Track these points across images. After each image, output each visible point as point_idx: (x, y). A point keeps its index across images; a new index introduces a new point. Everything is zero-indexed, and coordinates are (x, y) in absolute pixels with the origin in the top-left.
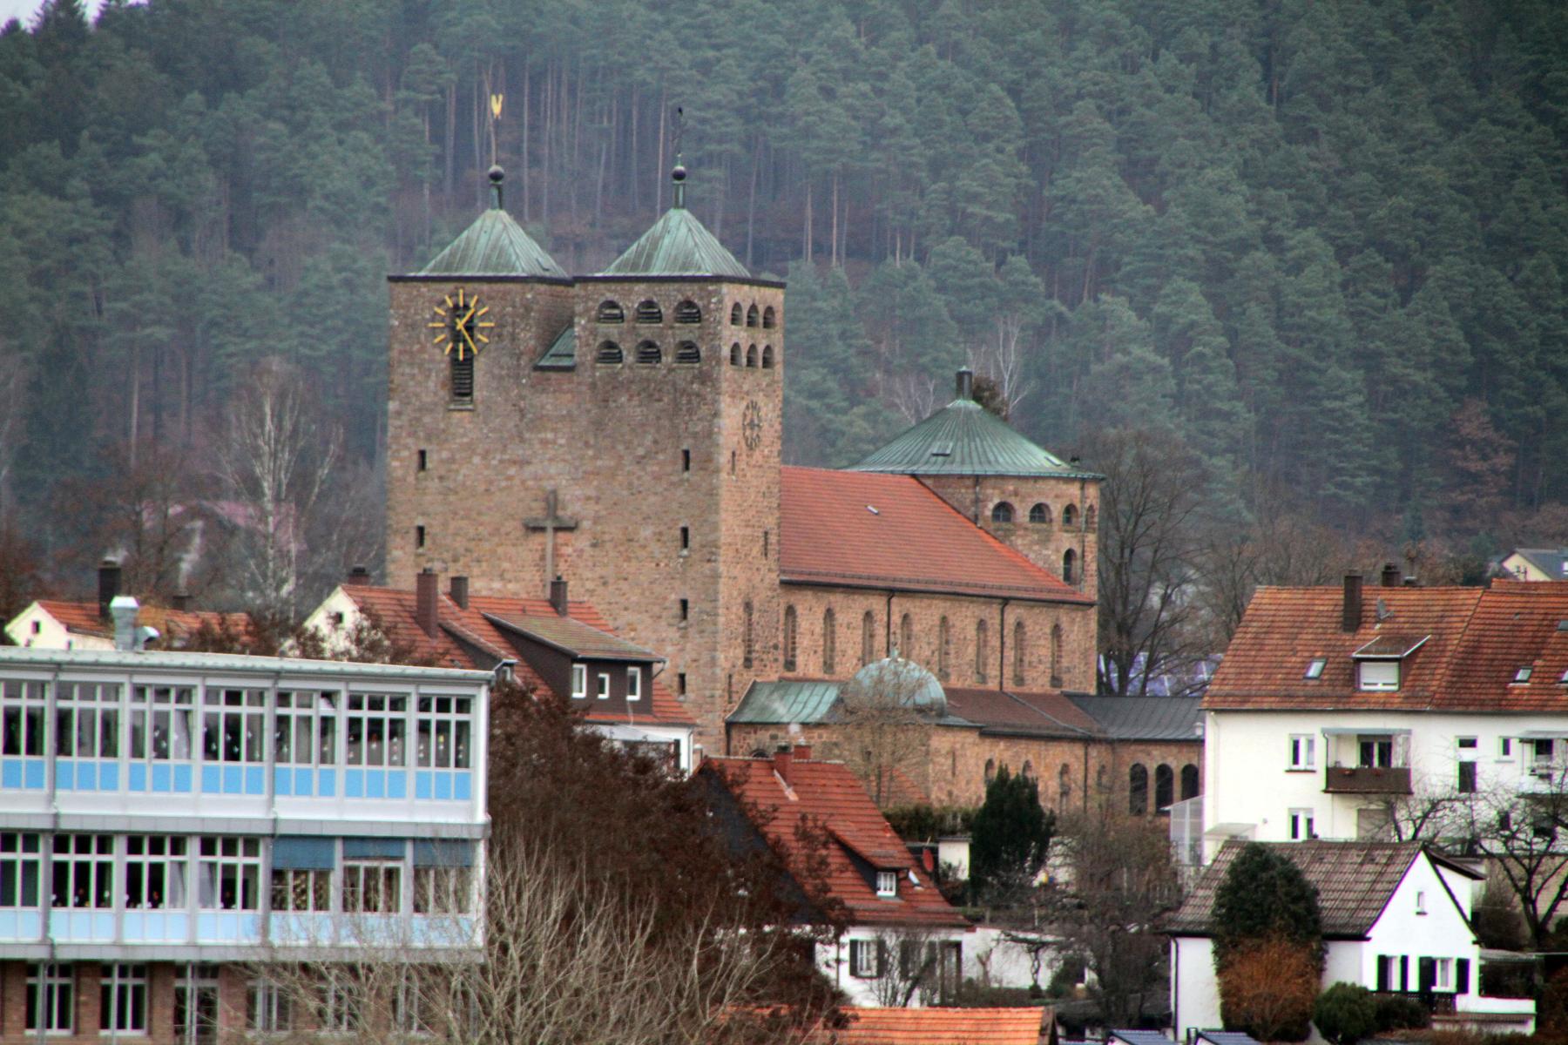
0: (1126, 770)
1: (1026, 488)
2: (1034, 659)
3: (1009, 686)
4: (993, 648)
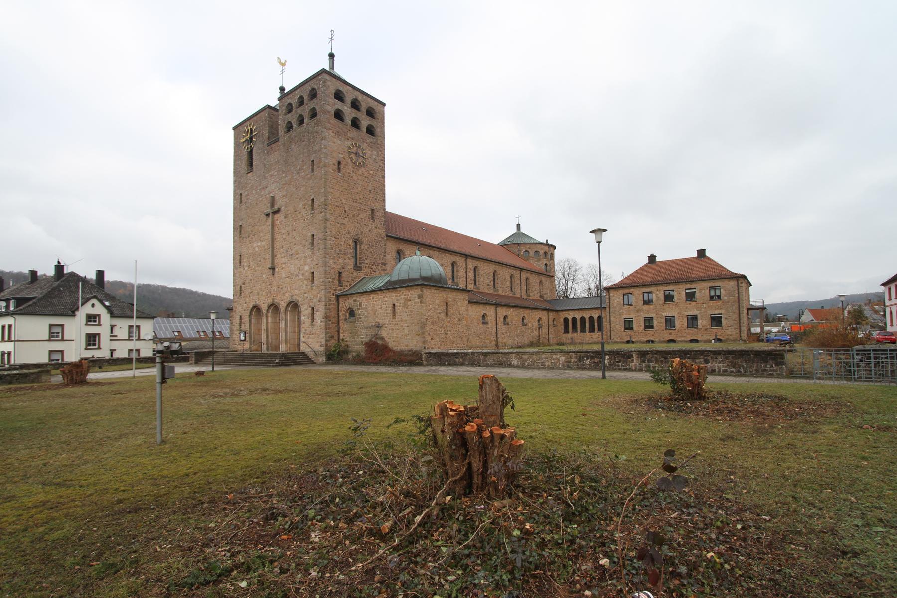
0: (562, 320)
2: (534, 289)
3: (524, 296)
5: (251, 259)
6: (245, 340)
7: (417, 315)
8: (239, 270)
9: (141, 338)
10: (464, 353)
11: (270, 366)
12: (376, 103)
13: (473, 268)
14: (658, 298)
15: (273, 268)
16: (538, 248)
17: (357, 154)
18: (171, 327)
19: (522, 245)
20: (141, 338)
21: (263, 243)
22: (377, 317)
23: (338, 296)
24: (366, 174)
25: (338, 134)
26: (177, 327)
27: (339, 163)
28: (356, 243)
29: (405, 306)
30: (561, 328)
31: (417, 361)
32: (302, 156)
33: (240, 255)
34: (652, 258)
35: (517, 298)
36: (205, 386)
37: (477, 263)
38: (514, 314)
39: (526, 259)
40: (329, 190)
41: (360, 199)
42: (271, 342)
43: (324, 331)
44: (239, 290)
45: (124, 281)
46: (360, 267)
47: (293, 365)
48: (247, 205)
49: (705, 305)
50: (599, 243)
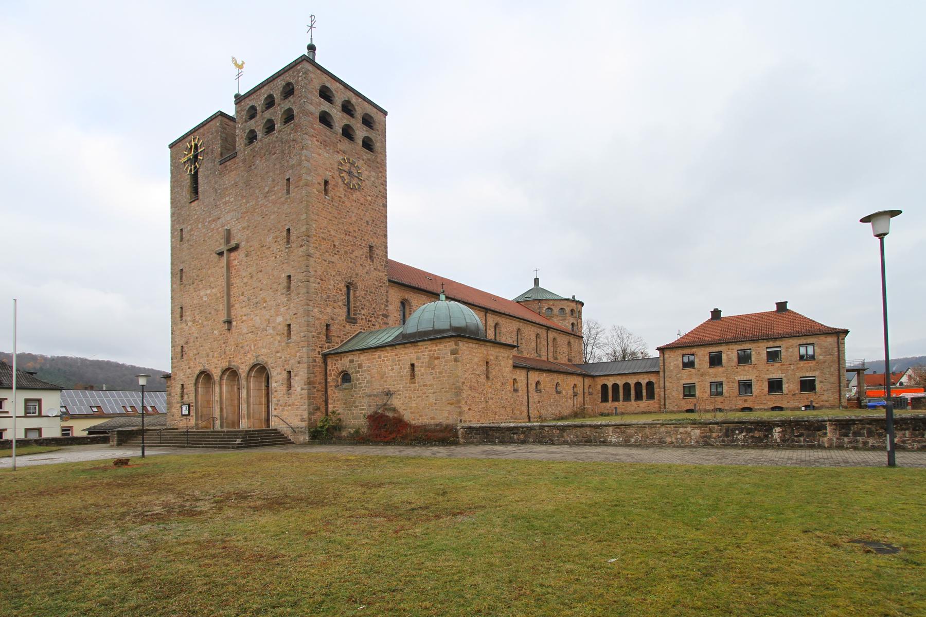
0: (599, 387)
1: (556, 303)
2: (561, 352)
3: (551, 359)
5: (197, 312)
6: (189, 414)
7: (449, 377)
8: (180, 327)
9: (43, 414)
11: (229, 448)
12: (375, 110)
13: (493, 325)
14: (729, 359)
15: (229, 322)
16: (564, 305)
17: (350, 173)
18: (88, 401)
20: (43, 414)
21: (213, 290)
22: (385, 381)
23: (325, 356)
24: (362, 200)
25: (324, 144)
26: (95, 401)
27: (326, 183)
28: (348, 288)
29: (431, 366)
31: (452, 439)
32: (271, 174)
33: (182, 308)
34: (716, 314)
35: (543, 361)
36: (129, 485)
37: (498, 319)
39: (549, 318)
41: (355, 231)
42: (227, 416)
43: (306, 401)
44: (180, 353)
45: (34, 354)
46: (354, 319)
47: (263, 446)
48: (191, 243)
49: (792, 367)
50: (881, 236)
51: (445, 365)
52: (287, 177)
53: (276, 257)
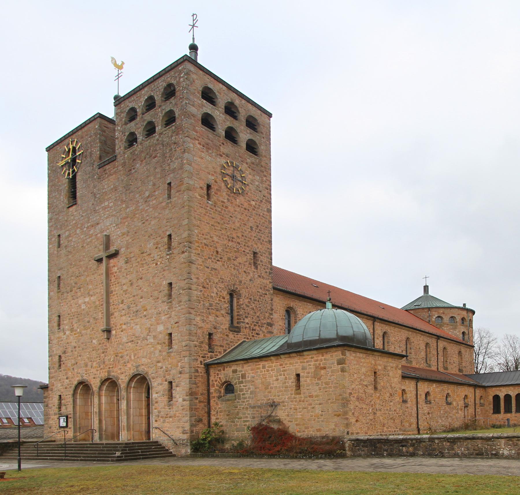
0: (491, 398)
1: (446, 311)
2: (452, 361)
3: (441, 369)
4: (433, 354)
6: (67, 426)
7: (336, 387)
10: (416, 439)
11: (108, 461)
12: (259, 112)
13: (381, 334)
19: (433, 310)
21: (92, 298)
22: (270, 392)
23: (208, 366)
24: (246, 205)
25: (207, 147)
27: (209, 187)
28: (231, 295)
29: (316, 376)
30: (490, 408)
31: (338, 452)
32: (152, 178)
33: (59, 316)
38: (437, 390)
39: (439, 326)
40: (195, 222)
41: (238, 237)
43: (188, 413)
46: (237, 327)
47: (143, 458)
48: (69, 249)
51: (331, 376)
52: (168, 182)
53: (157, 264)
